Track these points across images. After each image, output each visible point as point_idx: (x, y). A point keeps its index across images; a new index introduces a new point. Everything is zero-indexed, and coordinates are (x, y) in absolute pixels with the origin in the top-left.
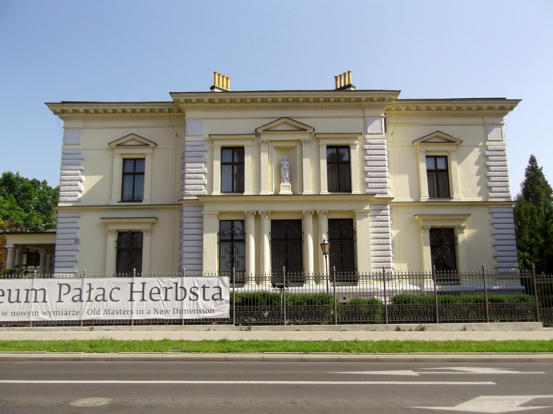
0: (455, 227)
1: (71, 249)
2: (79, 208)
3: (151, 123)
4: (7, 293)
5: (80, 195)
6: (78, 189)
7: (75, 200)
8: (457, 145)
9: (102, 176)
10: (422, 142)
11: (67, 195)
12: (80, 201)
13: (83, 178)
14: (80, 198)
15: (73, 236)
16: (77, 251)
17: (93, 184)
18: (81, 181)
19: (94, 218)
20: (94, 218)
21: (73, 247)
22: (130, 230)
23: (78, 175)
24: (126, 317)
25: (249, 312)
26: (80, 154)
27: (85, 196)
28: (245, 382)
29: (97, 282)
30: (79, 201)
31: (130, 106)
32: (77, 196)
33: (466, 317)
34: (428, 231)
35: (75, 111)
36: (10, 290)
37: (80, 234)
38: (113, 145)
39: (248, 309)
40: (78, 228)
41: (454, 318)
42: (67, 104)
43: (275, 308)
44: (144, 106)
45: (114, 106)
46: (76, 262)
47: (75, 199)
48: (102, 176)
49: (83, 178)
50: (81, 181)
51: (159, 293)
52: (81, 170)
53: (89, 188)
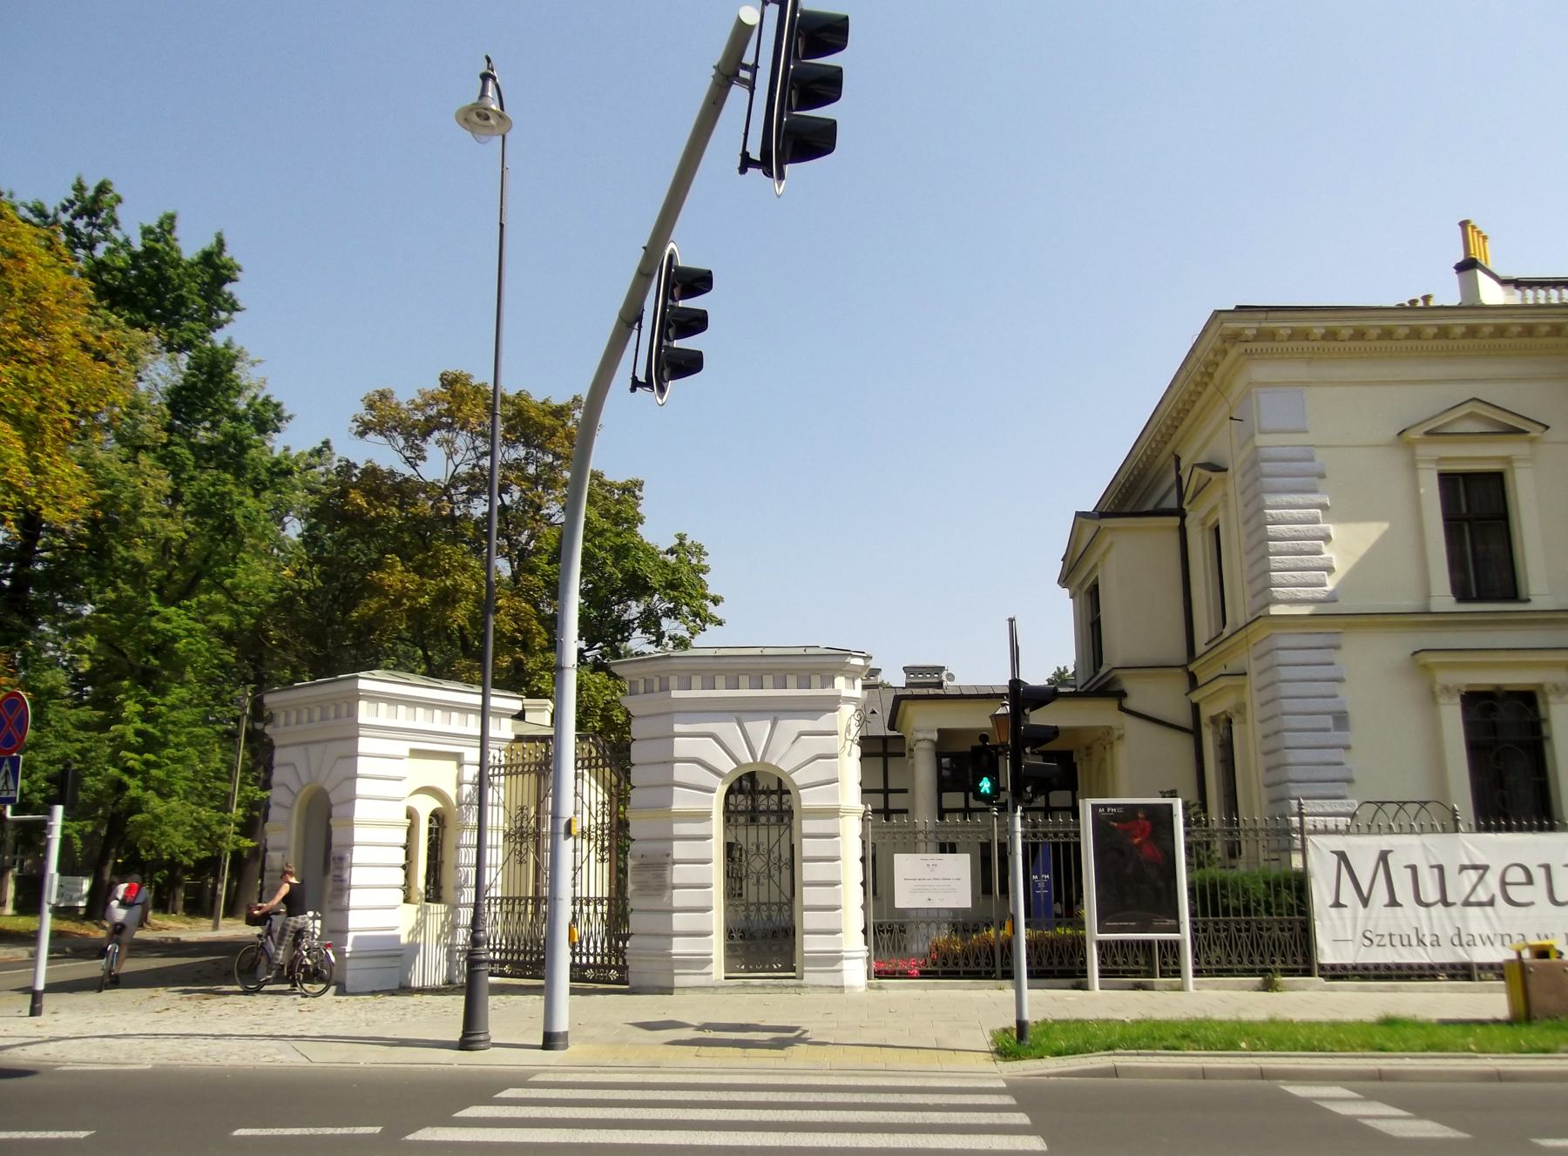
0: (1541, 686)
1: (1331, 743)
2: (1333, 621)
3: (1405, 370)
4: (1539, 876)
5: (1331, 583)
6: (1321, 563)
7: (1322, 596)
8: (1532, 441)
9: (1385, 526)
10: (1428, 433)
11: (1293, 581)
12: (1335, 601)
13: (1332, 529)
14: (1333, 592)
15: (1330, 705)
16: (1347, 748)
17: (1361, 549)
18: (1327, 538)
19: (1394, 647)
20: (1394, 647)
21: (1335, 737)
22: (1498, 687)
23: (1316, 521)
24: (1400, 955)
25: (1223, 935)
26: (1312, 460)
27: (1342, 584)
28: (51, 1135)
29: (1409, 848)
30: (1331, 599)
31: (1467, 316)
32: (1324, 585)
33: (1130, 959)
34: (1458, 700)
35: (1360, 335)
36: (1547, 868)
37: (1349, 697)
38: (1417, 434)
39: (1243, 926)
40: (1339, 680)
41: (1295, 962)
42: (1279, 314)
43: (1216, 923)
44: (1510, 316)
45: (1440, 317)
46: (1350, 781)
47: (1318, 592)
48: (1385, 526)
49: (1332, 529)
50: (1327, 538)
51: (1530, 881)
52: (1323, 507)
53: (1353, 560)
